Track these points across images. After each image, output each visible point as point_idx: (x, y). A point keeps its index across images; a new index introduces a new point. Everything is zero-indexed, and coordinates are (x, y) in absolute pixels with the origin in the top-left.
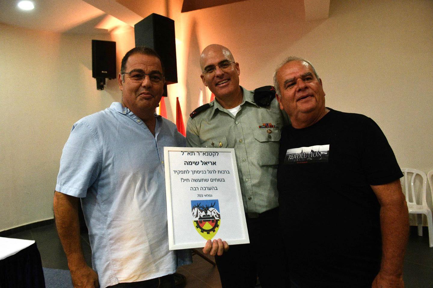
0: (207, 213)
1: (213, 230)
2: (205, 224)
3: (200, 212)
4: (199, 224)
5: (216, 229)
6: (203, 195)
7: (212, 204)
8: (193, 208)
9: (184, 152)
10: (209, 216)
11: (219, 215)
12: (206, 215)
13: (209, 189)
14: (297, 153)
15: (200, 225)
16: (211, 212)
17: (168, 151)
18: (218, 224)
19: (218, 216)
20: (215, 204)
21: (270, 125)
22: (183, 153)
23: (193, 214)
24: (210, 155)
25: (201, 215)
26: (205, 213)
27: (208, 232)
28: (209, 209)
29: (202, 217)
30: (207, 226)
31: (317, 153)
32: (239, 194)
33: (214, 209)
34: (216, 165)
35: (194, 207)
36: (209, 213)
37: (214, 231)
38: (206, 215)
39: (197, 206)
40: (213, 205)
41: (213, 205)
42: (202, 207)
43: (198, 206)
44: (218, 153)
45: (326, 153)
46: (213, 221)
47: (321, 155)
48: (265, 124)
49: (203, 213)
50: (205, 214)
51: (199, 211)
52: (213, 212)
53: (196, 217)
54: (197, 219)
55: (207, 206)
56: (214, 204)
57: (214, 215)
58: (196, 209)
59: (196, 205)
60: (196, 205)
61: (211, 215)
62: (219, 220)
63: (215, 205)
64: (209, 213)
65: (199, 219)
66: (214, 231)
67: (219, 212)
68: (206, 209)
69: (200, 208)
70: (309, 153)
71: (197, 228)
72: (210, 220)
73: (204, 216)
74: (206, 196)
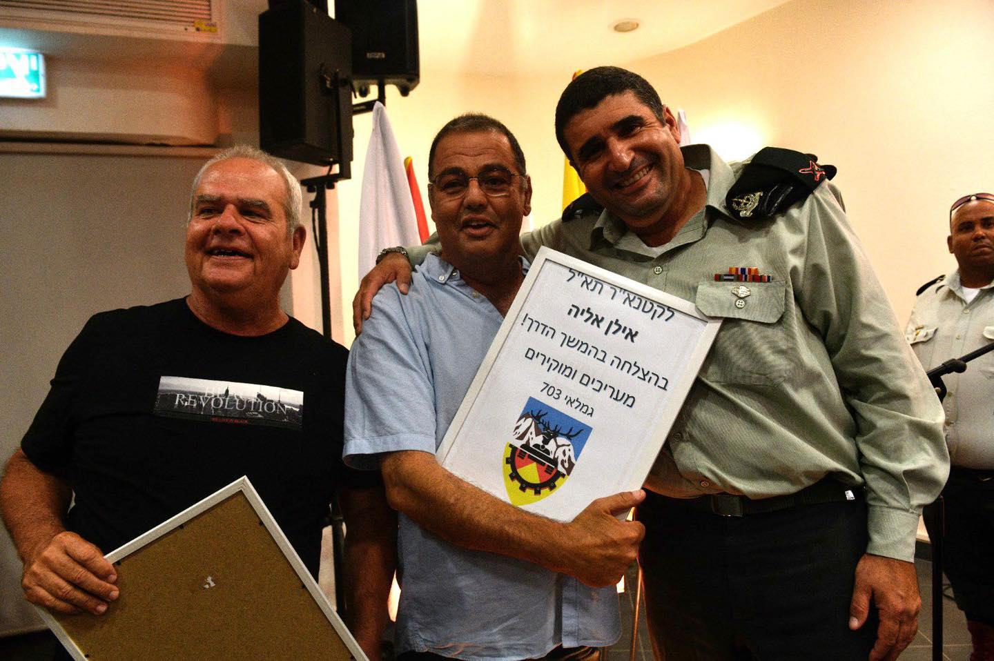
0: (547, 444)
1: (537, 489)
2: (531, 465)
3: (534, 433)
4: (515, 458)
5: (545, 491)
6: (562, 396)
7: (571, 430)
8: (525, 415)
9: (577, 274)
10: (547, 452)
11: (571, 465)
12: (543, 447)
13: (614, 396)
14: (207, 392)
15: (517, 459)
16: (558, 446)
17: (546, 259)
18: (556, 483)
19: (566, 465)
20: (578, 433)
22: (572, 275)
23: (517, 428)
24: (643, 311)
25: (530, 441)
26: (543, 442)
27: (538, 489)
28: (558, 438)
29: (531, 446)
30: (531, 472)
31: (276, 405)
32: (886, 465)
33: (569, 445)
34: (632, 341)
35: (528, 413)
36: (551, 446)
37: (538, 493)
38: (543, 447)
39: (535, 415)
40: (572, 434)
41: (572, 434)
42: (544, 425)
43: (537, 418)
44: (673, 314)
45: (298, 410)
46: (549, 470)
47: (287, 412)
49: (539, 440)
50: (541, 444)
51: (532, 429)
52: (561, 449)
53: (518, 438)
54: (518, 444)
55: (558, 428)
56: (578, 434)
57: (561, 457)
58: (530, 420)
59: (536, 413)
60: (536, 413)
61: (553, 453)
62: (563, 476)
63: (576, 437)
64: (551, 446)
65: (523, 446)
66: (538, 493)
67: (576, 460)
68: (550, 434)
69: (540, 423)
70: (253, 401)
71: (507, 462)
72: (543, 464)
73: (537, 446)
74: (570, 402)
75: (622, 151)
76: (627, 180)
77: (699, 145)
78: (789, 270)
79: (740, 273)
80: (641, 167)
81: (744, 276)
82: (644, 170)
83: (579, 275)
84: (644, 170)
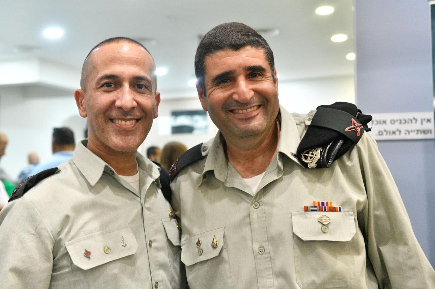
21: (329, 205)
48: (319, 203)
75: (245, 88)
76: (242, 110)
77: (344, 102)
78: (355, 203)
79: (321, 205)
80: (254, 104)
81: (324, 207)
82: (255, 107)
83: (387, 134)
84: (255, 107)
